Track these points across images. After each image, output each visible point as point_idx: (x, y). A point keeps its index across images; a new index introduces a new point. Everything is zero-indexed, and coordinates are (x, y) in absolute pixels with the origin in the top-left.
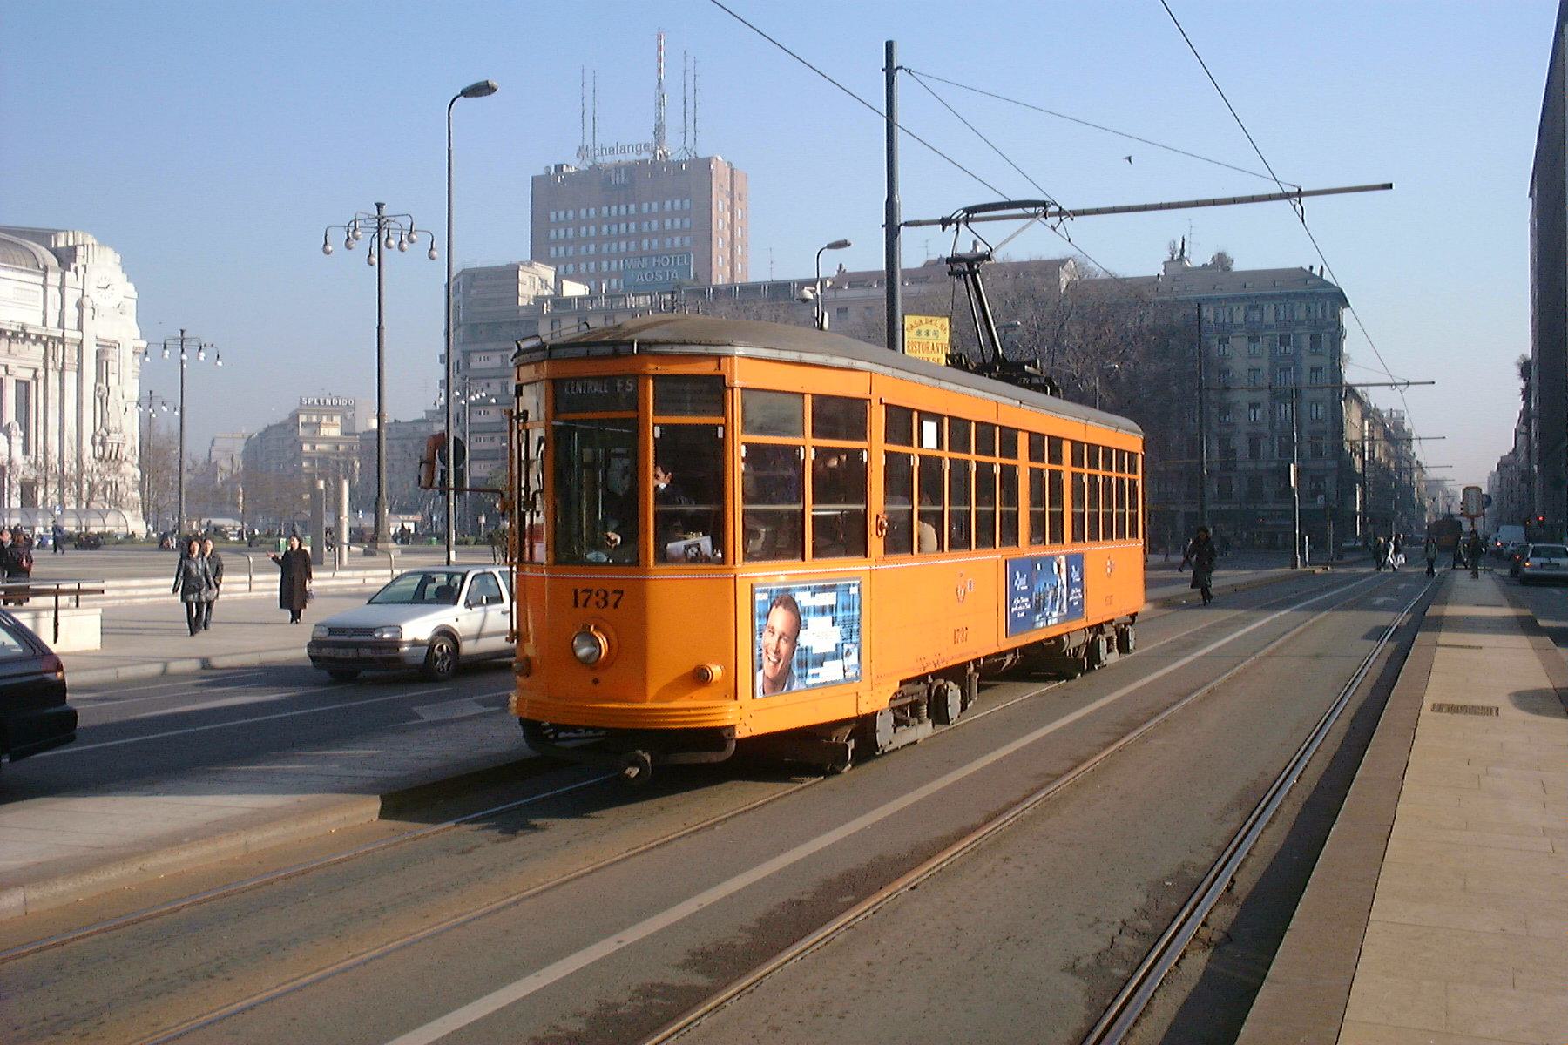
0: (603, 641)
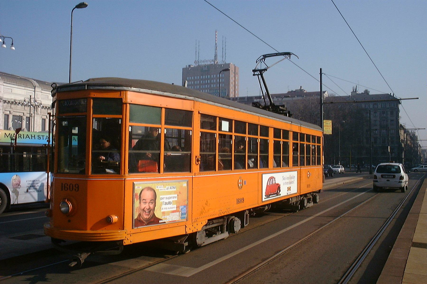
0: (70, 205)
